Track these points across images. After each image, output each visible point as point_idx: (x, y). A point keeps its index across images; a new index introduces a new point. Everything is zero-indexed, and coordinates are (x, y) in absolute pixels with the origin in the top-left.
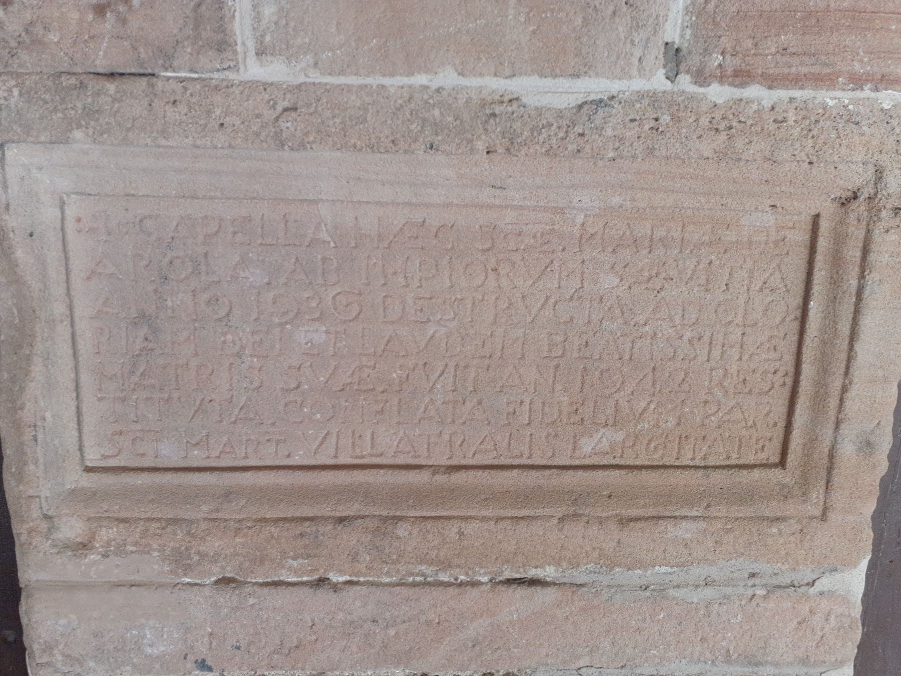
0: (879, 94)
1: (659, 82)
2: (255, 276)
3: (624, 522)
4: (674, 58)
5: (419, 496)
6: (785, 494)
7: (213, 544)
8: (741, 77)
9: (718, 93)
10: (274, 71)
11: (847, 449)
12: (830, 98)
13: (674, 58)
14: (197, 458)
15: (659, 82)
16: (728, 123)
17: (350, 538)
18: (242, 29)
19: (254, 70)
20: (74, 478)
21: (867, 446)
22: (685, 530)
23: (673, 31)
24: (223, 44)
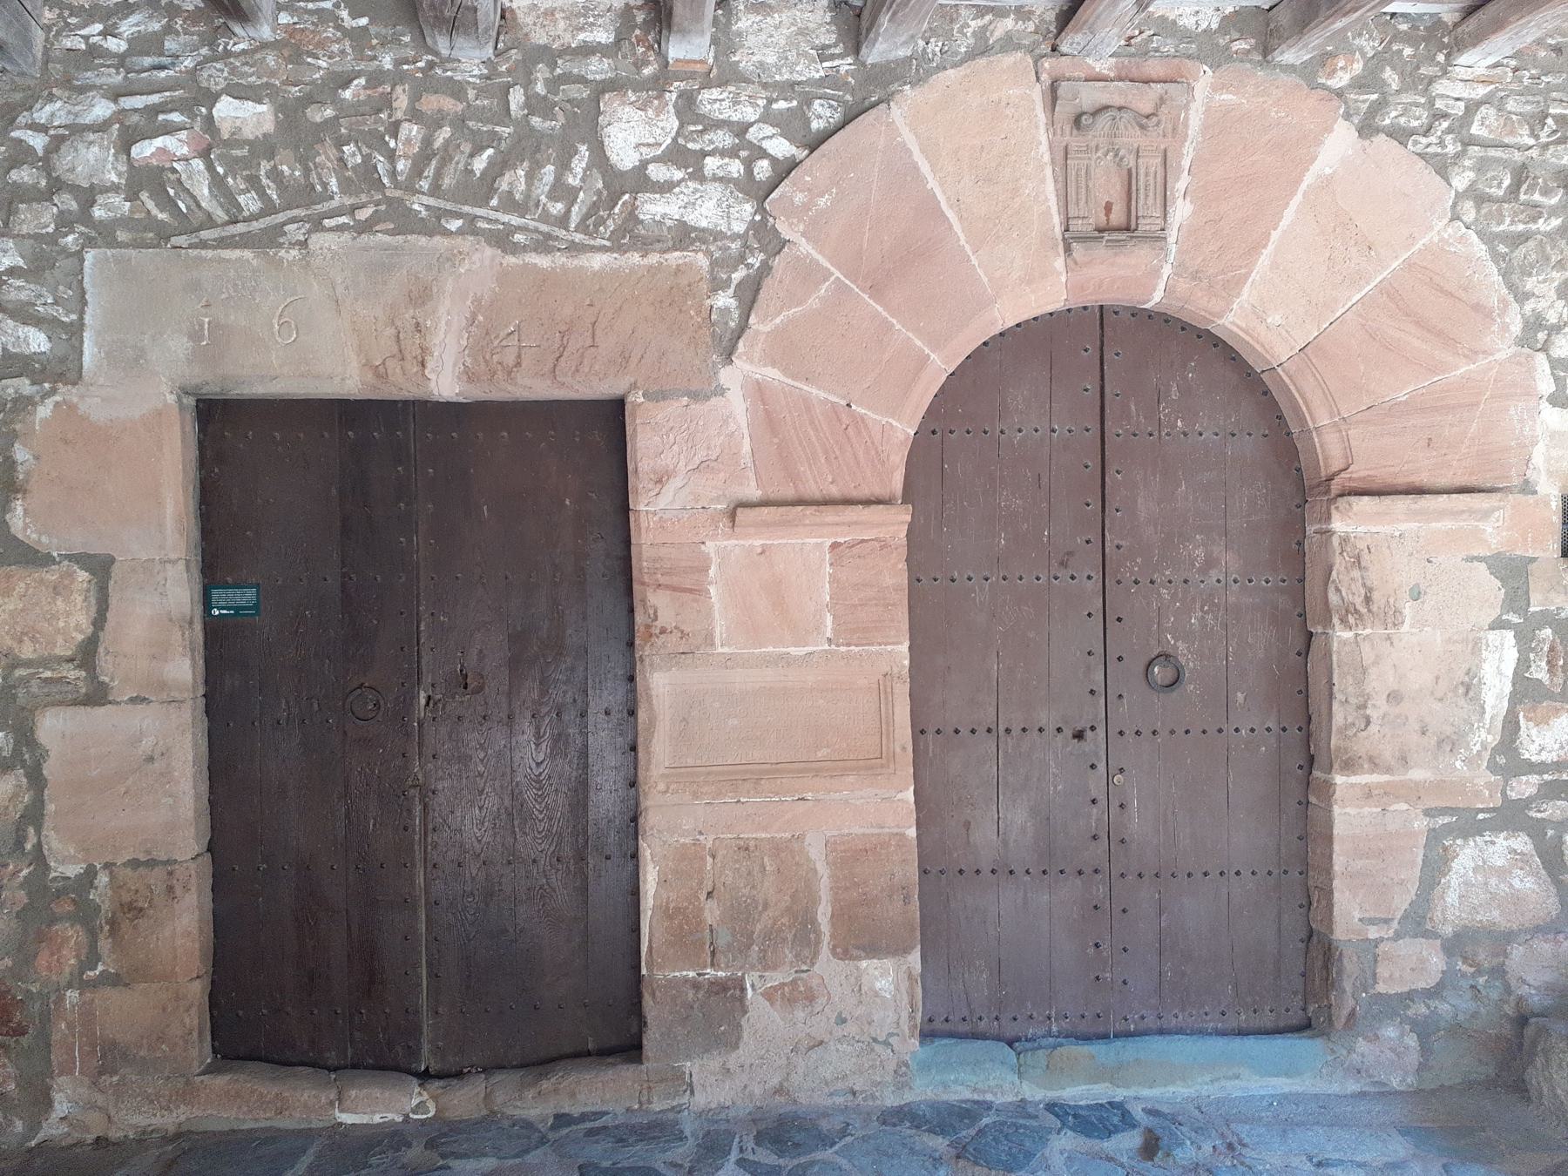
0: (687, 1133)
1: (826, 647)
2: (717, 705)
3: (1331, 695)
4: (829, 640)
5: (768, 772)
6: (882, 766)
7: (705, 790)
8: (849, 645)
9: (843, 649)
10: (726, 650)
11: (898, 750)
12: (873, 648)
13: (829, 640)
14: (699, 763)
15: (826, 647)
16: (847, 657)
17: (748, 785)
18: (717, 641)
19: (720, 650)
20: (662, 771)
21: (904, 749)
22: (851, 779)
23: (829, 634)
24: (713, 644)
